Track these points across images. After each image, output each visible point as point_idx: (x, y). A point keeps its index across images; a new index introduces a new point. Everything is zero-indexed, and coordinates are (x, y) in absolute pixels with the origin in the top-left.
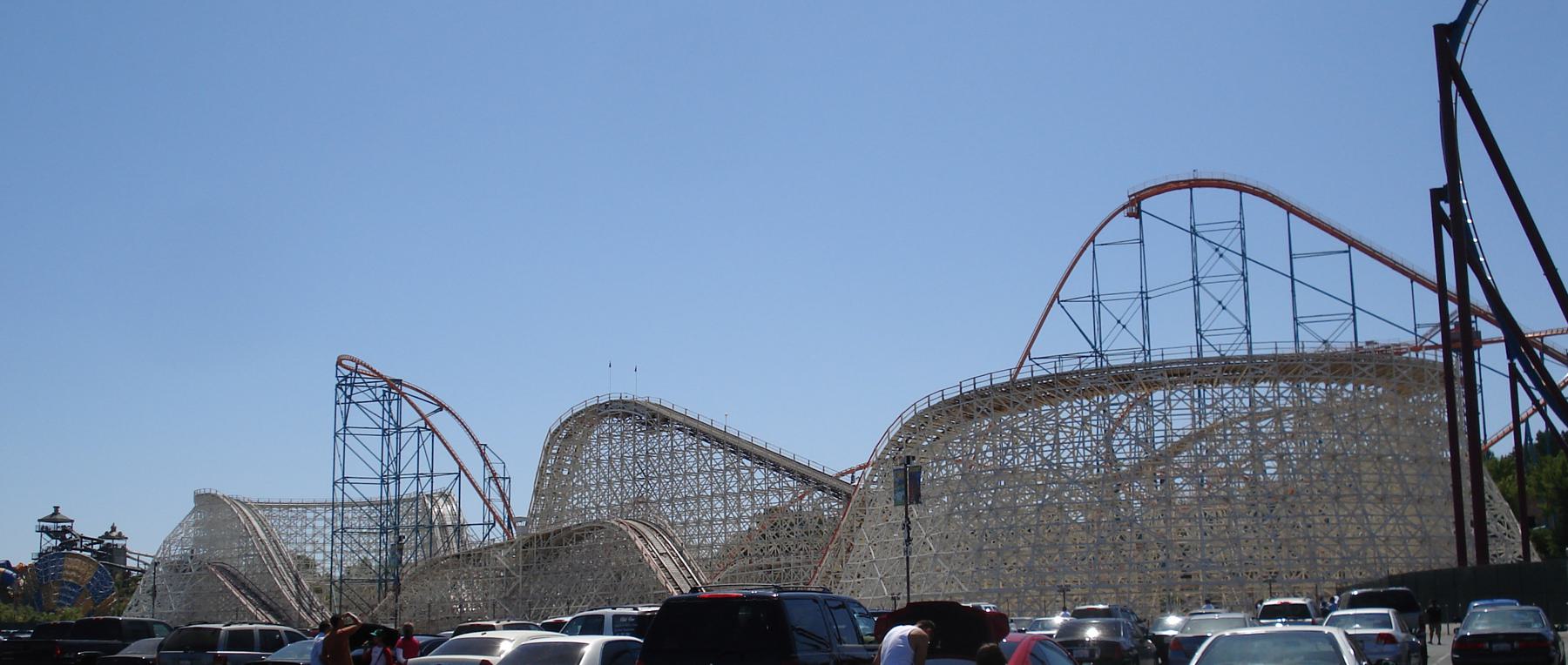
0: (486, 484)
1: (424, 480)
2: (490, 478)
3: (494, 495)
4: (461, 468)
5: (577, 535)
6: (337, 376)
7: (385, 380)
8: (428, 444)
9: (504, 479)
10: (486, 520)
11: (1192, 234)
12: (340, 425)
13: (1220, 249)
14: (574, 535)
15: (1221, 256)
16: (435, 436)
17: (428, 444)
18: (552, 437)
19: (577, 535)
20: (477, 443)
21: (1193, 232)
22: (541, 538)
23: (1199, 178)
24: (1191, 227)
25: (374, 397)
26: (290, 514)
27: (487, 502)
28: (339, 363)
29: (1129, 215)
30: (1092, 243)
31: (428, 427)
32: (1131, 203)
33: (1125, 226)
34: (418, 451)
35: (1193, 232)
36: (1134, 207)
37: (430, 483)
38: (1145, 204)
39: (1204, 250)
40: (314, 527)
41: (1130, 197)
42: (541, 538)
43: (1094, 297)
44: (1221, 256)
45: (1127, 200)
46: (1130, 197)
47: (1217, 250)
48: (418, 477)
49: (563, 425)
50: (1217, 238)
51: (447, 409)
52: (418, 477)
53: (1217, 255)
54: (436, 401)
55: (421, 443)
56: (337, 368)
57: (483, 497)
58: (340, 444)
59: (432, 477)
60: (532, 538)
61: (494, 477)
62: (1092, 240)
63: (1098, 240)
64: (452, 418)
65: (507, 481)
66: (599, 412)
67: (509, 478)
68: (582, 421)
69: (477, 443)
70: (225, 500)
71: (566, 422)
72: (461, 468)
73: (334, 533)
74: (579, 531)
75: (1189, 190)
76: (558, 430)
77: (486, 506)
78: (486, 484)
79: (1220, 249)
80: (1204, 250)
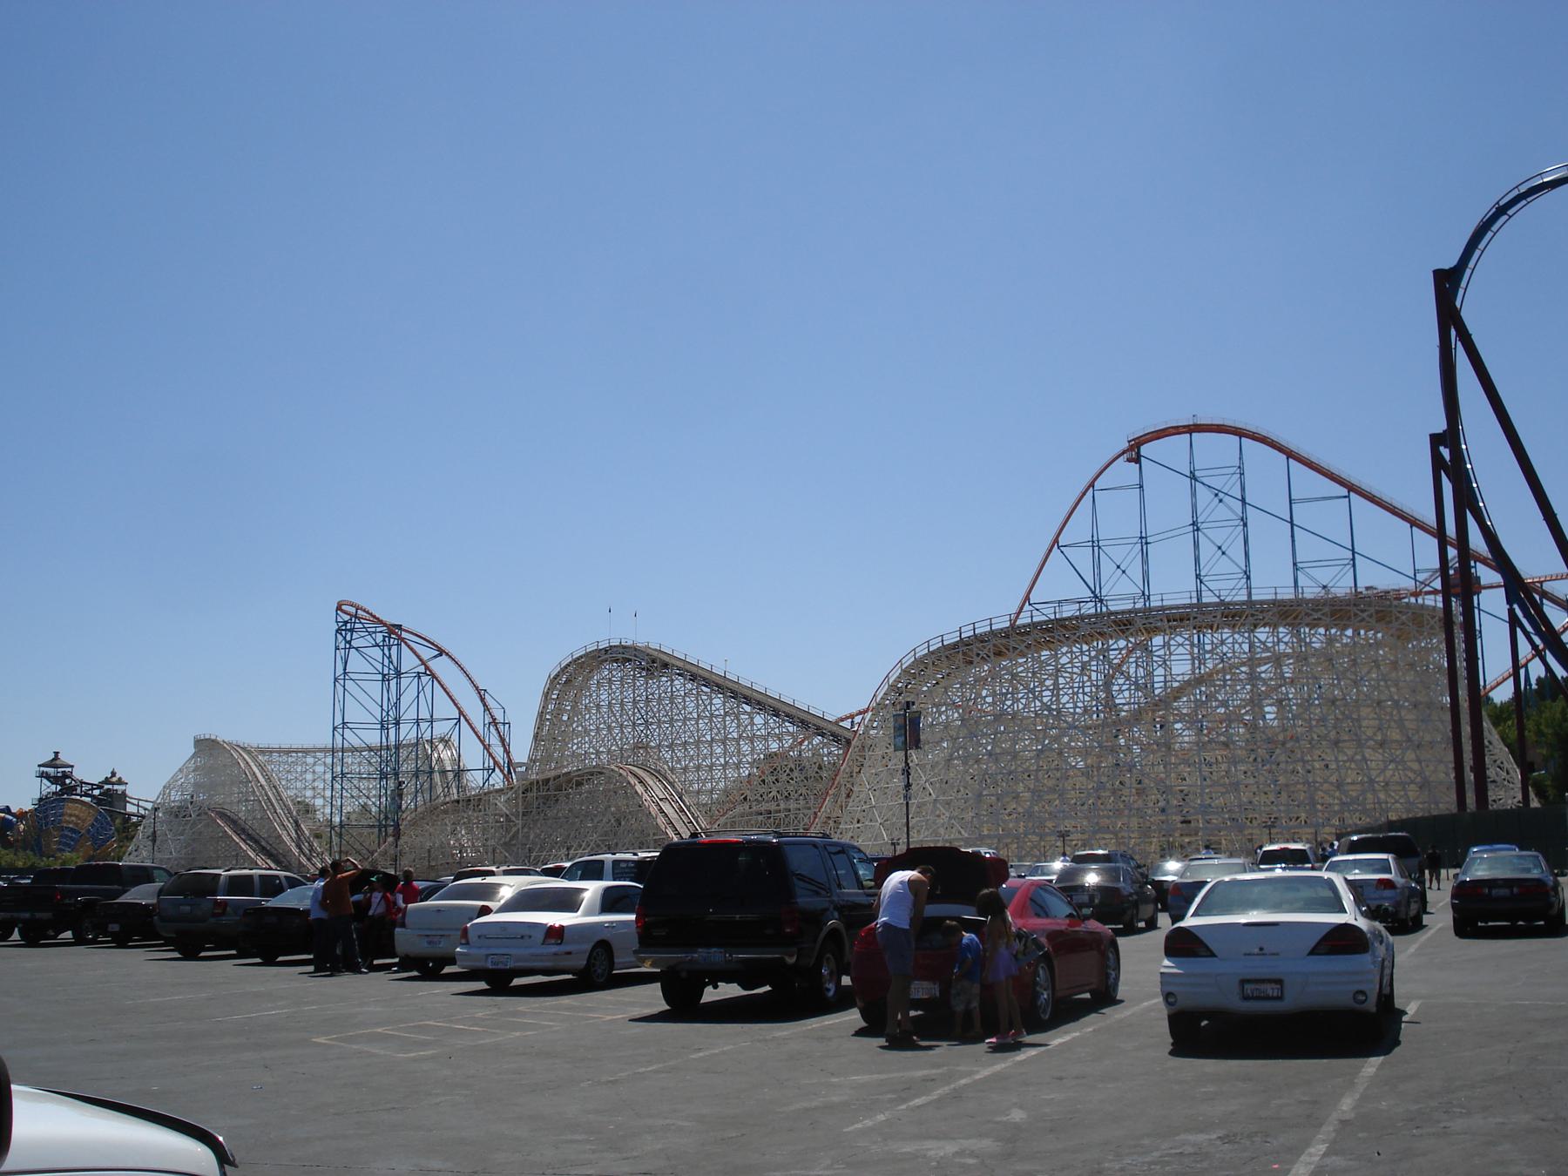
0: (486, 729)
1: (424, 726)
2: (490, 723)
3: (494, 740)
4: (461, 713)
5: (576, 781)
6: (337, 622)
7: (385, 625)
8: (428, 689)
9: (504, 724)
10: (486, 765)
11: (1191, 479)
12: (340, 671)
13: (1220, 494)
14: (574, 781)
15: (1221, 501)
16: (435, 682)
17: (428, 689)
18: (552, 682)
19: (576, 781)
20: (477, 688)
21: (1193, 477)
22: (541, 783)
23: (1199, 423)
24: (1191, 472)
25: (374, 643)
26: (290, 760)
27: (487, 747)
28: (339, 608)
29: (1129, 460)
30: (1091, 488)
31: (428, 672)
32: (1131, 448)
33: (1125, 471)
34: (418, 696)
35: (1193, 477)
36: (1134, 452)
37: (430, 728)
38: (1145, 450)
39: (1204, 495)
40: (314, 772)
41: (1129, 442)
42: (541, 783)
43: (1093, 542)
44: (1221, 501)
45: (1126, 445)
46: (1129, 442)
47: (1216, 495)
48: (418, 722)
49: (563, 670)
50: (1216, 483)
51: (447, 654)
52: (418, 722)
53: (1216, 500)
54: (436, 646)
55: (421, 688)
56: (337, 614)
57: (482, 742)
58: (340, 689)
59: (432, 722)
60: (532, 784)
61: (494, 722)
62: (1092, 485)
63: (1097, 485)
64: (465, 680)
65: (507, 726)
66: (599, 657)
67: (509, 723)
68: (582, 666)
69: (477, 688)
70: (225, 745)
71: (566, 667)
72: (461, 713)
73: (333, 778)
74: (579, 776)
75: (1188, 435)
76: (557, 675)
77: (486, 752)
78: (486, 729)
79: (1220, 494)
80: (1204, 495)
